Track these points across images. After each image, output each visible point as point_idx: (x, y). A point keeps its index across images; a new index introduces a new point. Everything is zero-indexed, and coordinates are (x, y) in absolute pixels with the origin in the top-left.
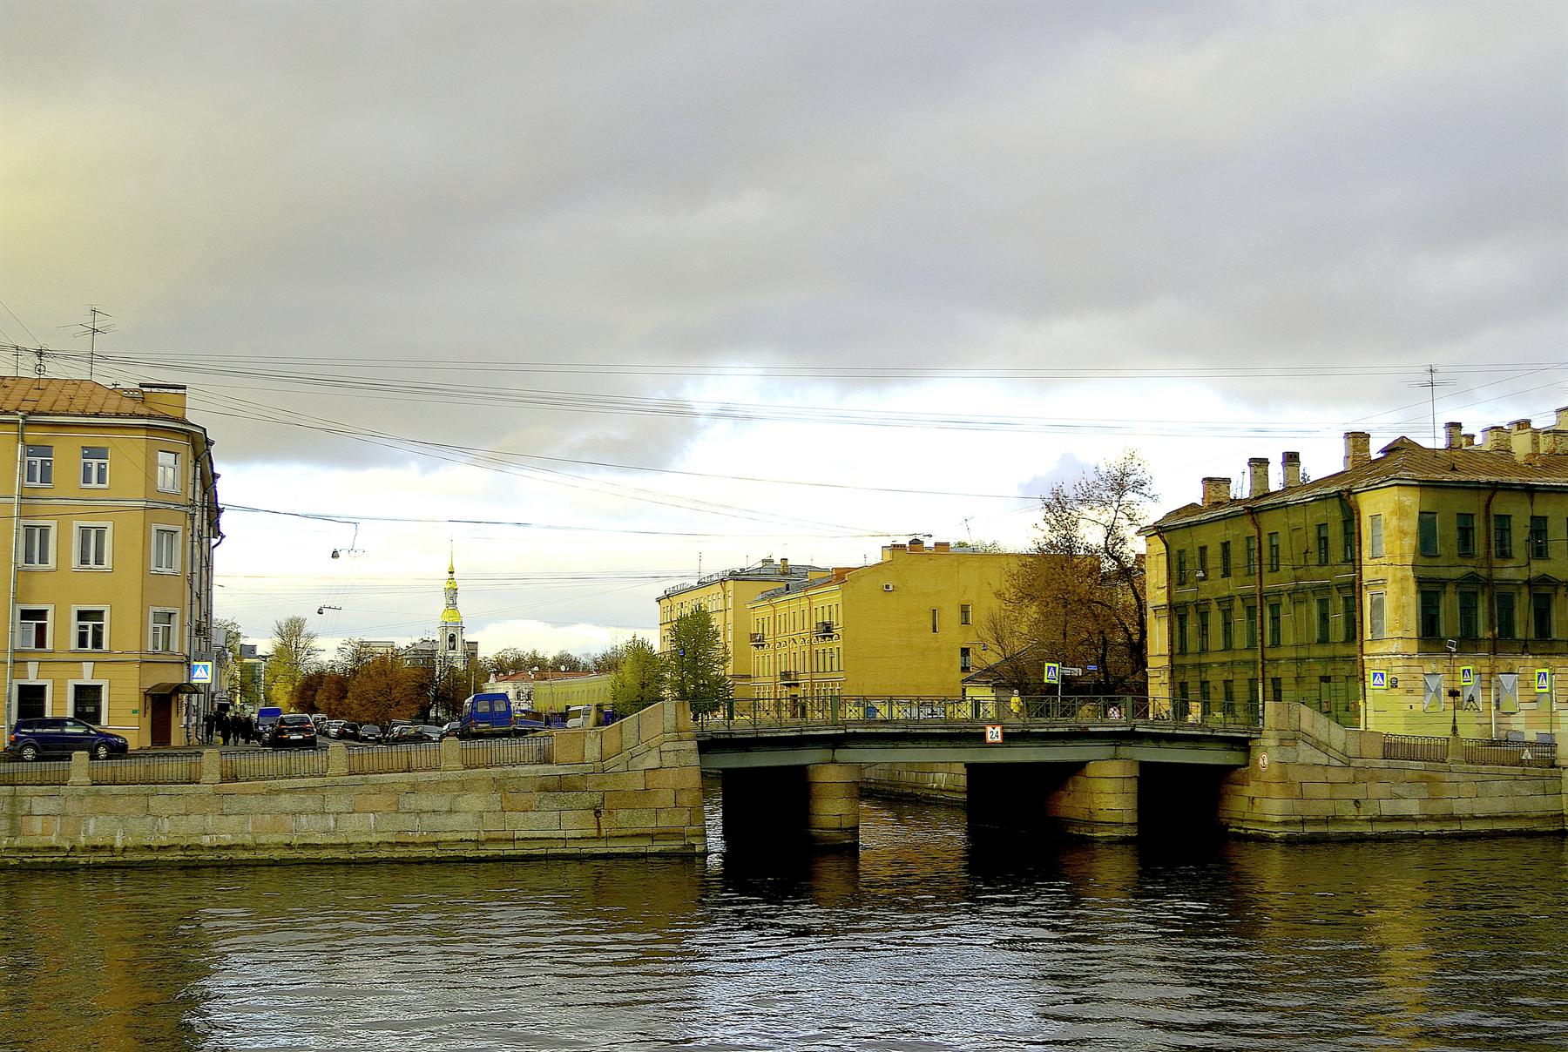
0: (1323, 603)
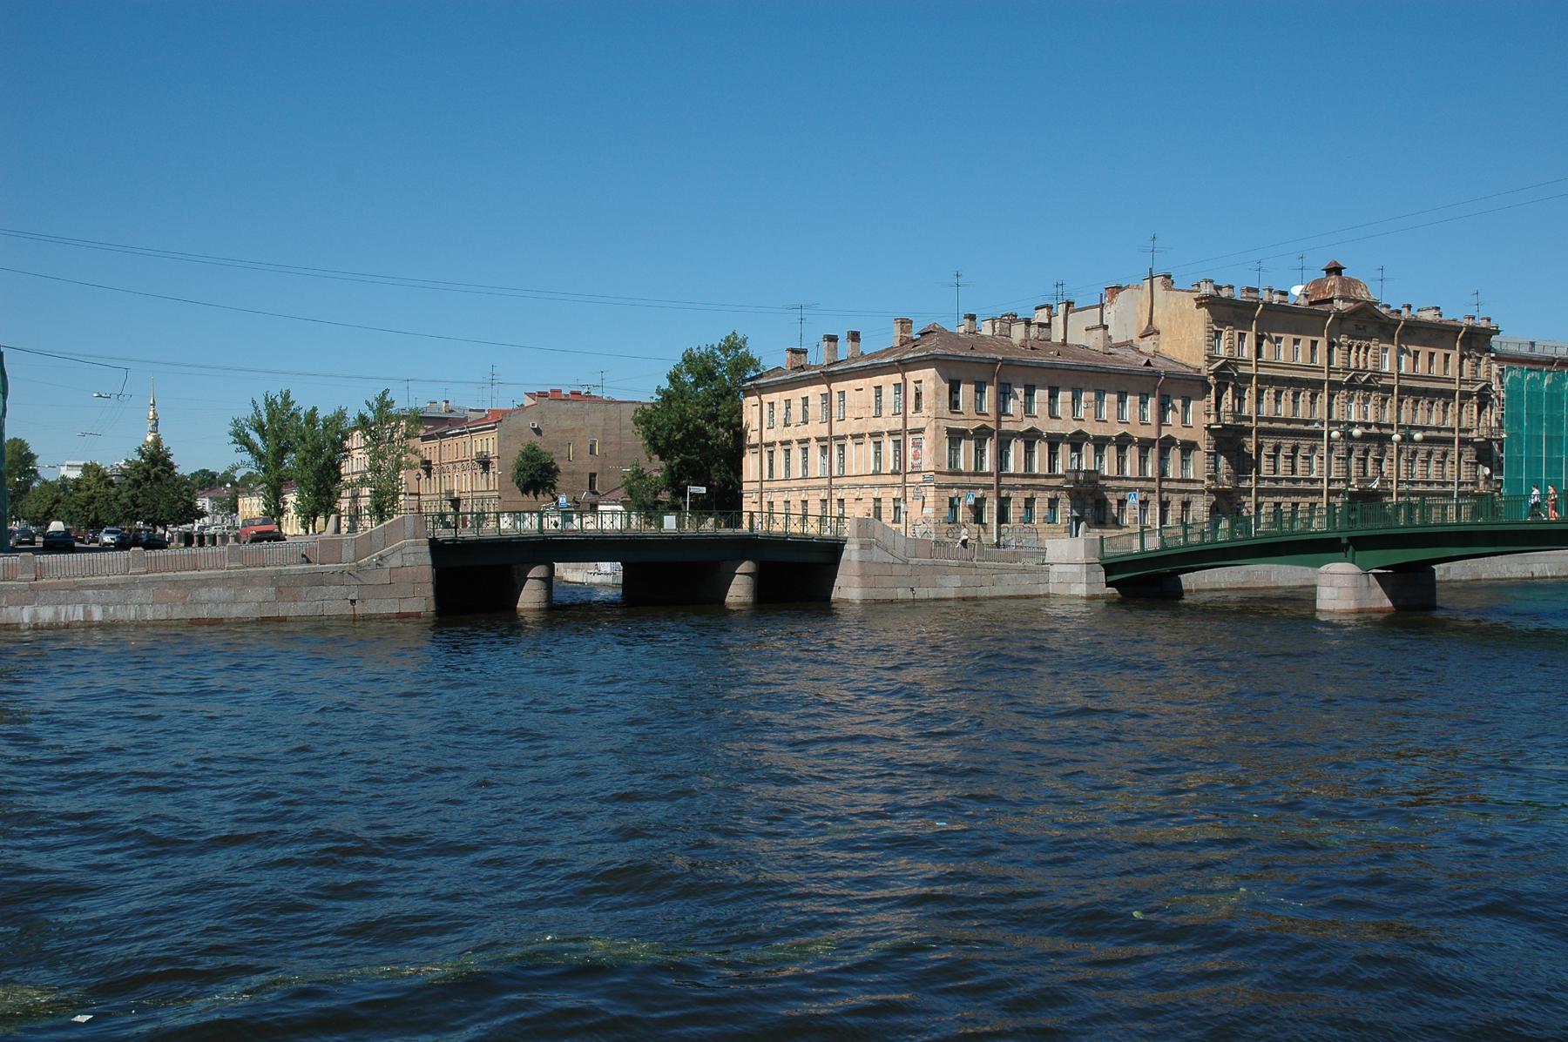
0: (878, 445)
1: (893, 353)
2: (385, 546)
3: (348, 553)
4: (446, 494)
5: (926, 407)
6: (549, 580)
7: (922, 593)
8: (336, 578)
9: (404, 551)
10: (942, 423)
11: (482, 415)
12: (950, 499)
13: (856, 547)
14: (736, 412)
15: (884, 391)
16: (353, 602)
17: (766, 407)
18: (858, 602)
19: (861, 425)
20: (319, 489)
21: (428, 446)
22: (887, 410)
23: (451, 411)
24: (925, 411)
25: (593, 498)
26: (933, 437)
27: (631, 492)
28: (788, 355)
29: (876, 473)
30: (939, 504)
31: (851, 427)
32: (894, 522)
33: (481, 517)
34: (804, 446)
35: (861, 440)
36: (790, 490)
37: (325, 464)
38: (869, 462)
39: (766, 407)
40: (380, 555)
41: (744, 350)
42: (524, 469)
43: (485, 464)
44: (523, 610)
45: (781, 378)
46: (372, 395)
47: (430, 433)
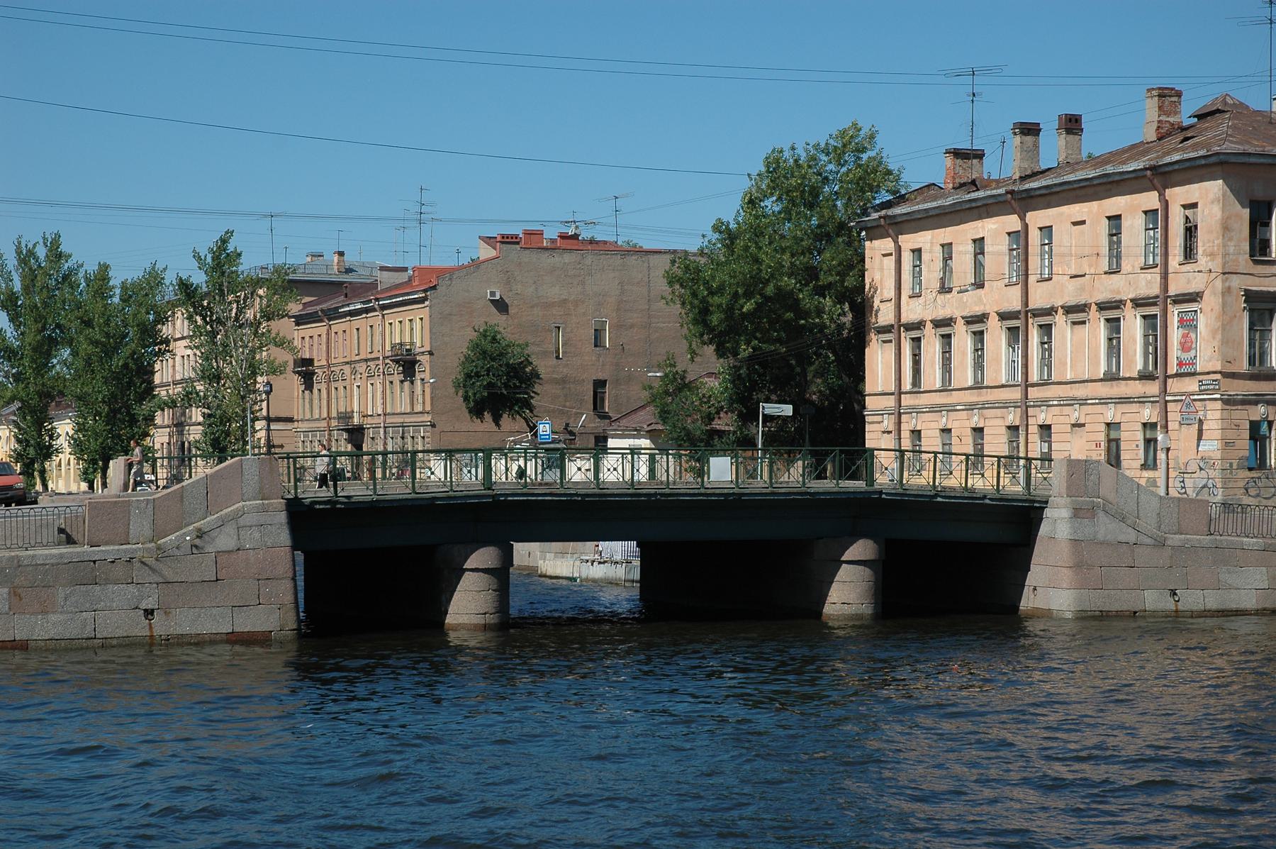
0: (1114, 324)
1: (1144, 153)
2: (208, 512)
3: (140, 526)
4: (339, 418)
5: (1205, 254)
6: (501, 574)
7: (1192, 600)
8: (119, 571)
9: (242, 522)
10: (1237, 282)
11: (403, 277)
12: (1252, 423)
13: (1065, 513)
14: (851, 267)
15: (1125, 223)
16: (149, 613)
17: (907, 258)
18: (1069, 615)
19: (1082, 289)
20: (114, 412)
21: (302, 333)
22: (1130, 263)
23: (349, 271)
24: (1203, 261)
25: (598, 425)
26: (1218, 308)
27: (664, 415)
28: (949, 161)
29: (1111, 377)
30: (1231, 434)
31: (1068, 293)
32: (1144, 467)
33: (410, 460)
34: (977, 327)
35: (1080, 317)
36: (951, 409)
37: (126, 366)
38: (1097, 357)
39: (907, 258)
40: (199, 530)
41: (871, 154)
42: (478, 375)
43: (407, 364)
44: (456, 628)
45: (934, 204)
46: (206, 243)
47: (310, 310)
